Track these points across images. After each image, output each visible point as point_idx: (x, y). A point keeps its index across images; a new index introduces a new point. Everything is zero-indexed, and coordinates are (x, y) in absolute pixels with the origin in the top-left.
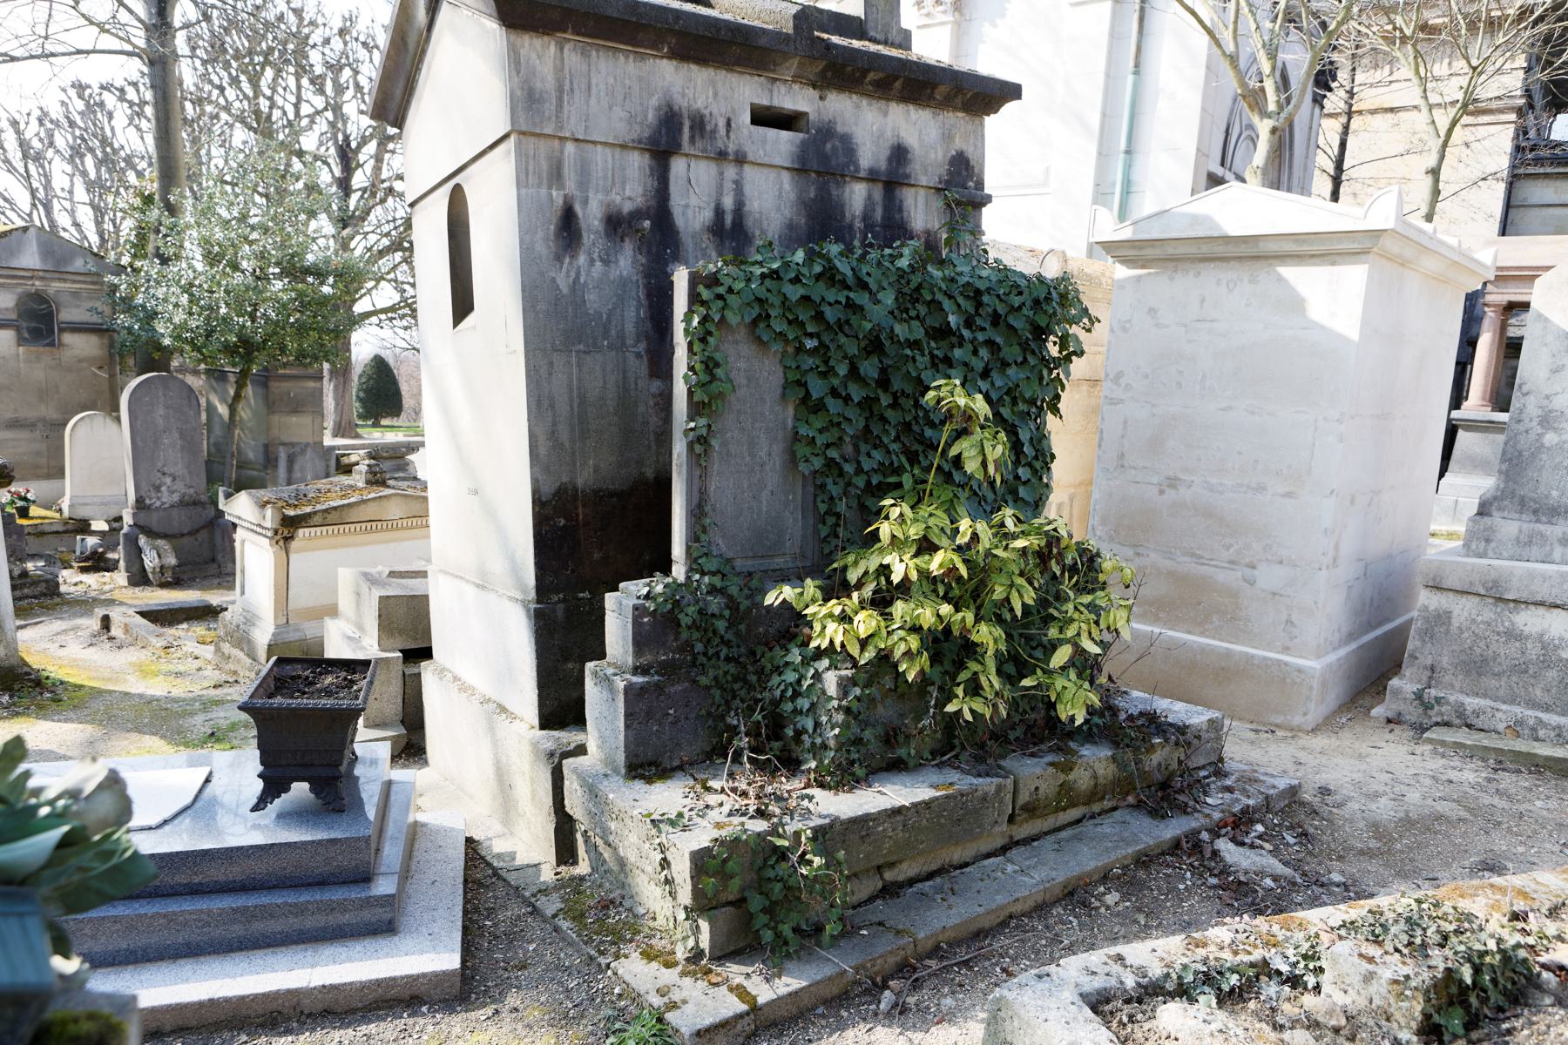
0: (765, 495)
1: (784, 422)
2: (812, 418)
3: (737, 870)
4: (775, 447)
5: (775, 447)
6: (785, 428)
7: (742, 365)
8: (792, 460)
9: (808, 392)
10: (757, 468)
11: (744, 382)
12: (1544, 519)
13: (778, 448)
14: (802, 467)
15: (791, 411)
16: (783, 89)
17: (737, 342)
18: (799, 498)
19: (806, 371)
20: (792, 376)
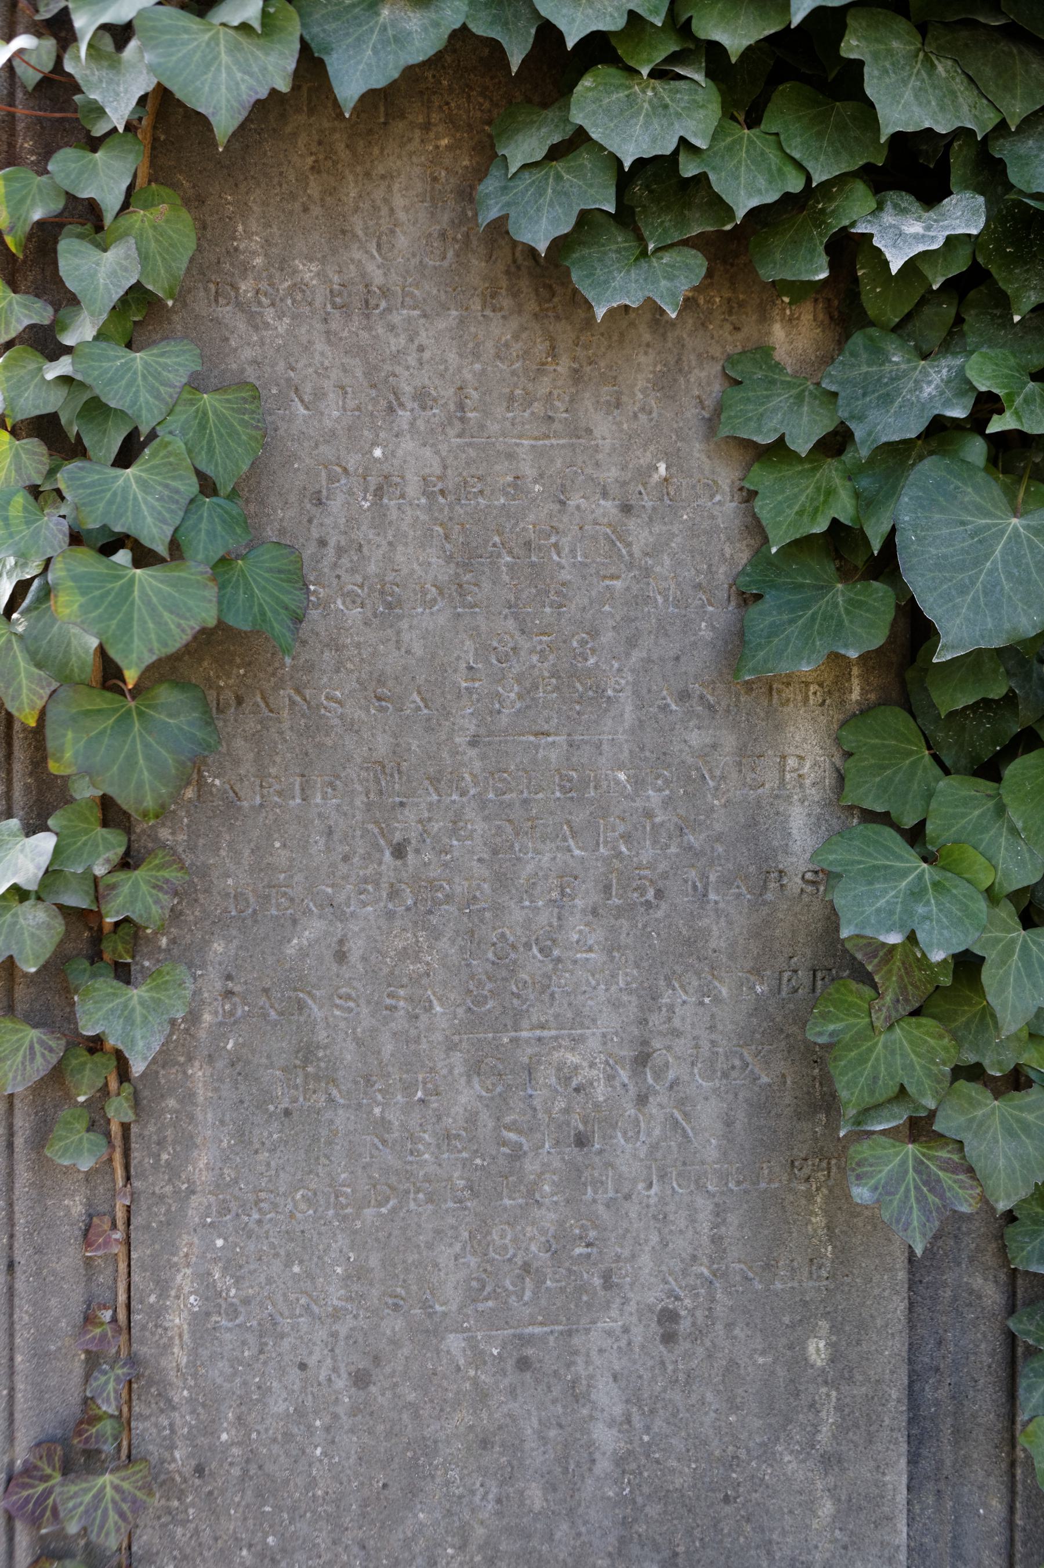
0: (610, 1345)
1: (756, 827)
2: (956, 805)
3: (822, 647)
4: (683, 1003)
5: (683, 1003)
6: (768, 874)
7: (412, 453)
8: (810, 1112)
9: (915, 630)
10: (545, 1158)
11: (424, 563)
12: (741, 579)
13: (708, 1017)
14: (885, 1173)
15: (806, 748)
16: (811, 317)
17: (364, 302)
18: (888, 1351)
19: (897, 456)
20: (798, 508)
